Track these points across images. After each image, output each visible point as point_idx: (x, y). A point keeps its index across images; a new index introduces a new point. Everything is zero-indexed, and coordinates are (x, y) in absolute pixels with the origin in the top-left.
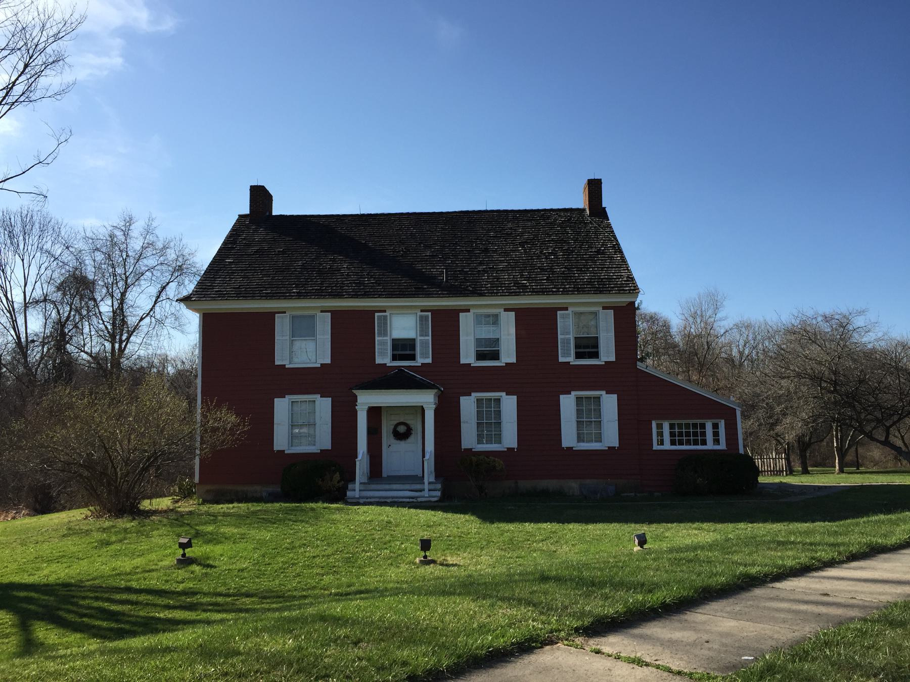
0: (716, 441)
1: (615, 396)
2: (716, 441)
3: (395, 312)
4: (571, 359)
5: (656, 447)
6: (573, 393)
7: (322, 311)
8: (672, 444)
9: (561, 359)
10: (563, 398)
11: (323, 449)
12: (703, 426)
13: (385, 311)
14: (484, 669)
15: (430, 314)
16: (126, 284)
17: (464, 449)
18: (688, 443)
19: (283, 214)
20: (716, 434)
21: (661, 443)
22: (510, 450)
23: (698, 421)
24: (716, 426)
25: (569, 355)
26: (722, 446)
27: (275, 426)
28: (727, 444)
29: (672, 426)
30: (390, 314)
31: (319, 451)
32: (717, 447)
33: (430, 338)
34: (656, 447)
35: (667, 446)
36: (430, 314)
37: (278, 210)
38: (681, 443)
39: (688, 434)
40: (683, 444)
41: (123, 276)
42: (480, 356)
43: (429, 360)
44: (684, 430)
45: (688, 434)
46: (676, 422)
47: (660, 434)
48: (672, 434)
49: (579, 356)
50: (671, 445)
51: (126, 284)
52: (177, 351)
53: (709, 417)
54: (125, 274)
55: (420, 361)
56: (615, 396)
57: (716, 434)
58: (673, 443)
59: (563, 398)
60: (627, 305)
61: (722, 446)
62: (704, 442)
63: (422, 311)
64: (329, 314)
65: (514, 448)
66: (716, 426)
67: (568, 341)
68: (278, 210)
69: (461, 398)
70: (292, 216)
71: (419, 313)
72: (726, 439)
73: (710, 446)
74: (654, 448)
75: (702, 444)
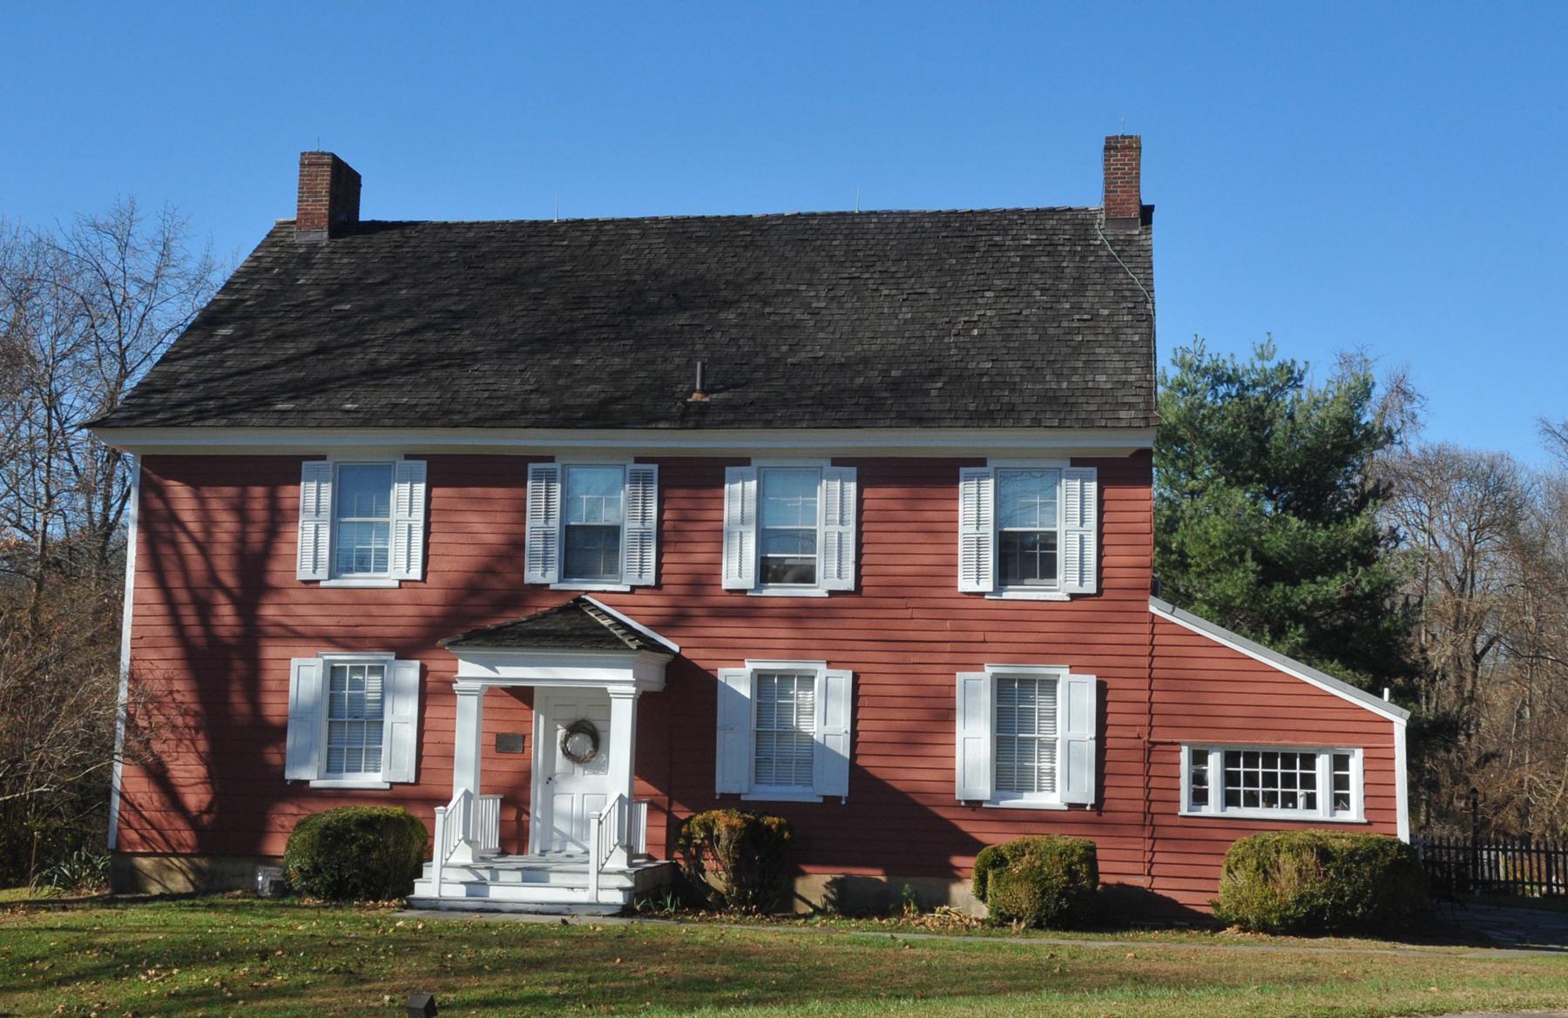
0: (1340, 801)
2: (1340, 801)
3: (574, 462)
7: (408, 457)
11: (726, 792)
13: (551, 459)
15: (655, 468)
16: (123, 365)
17: (722, 795)
19: (377, 219)
20: (1341, 782)
21: (1200, 797)
22: (831, 801)
26: (1355, 812)
27: (719, 734)
30: (563, 466)
31: (821, 800)
32: (1342, 816)
36: (655, 468)
37: (370, 209)
38: (1252, 801)
39: (1270, 780)
41: (115, 348)
45: (1270, 780)
47: (1199, 779)
48: (1230, 779)
51: (123, 365)
54: (120, 343)
57: (1341, 782)
58: (1230, 799)
60: (1131, 456)
61: (1355, 812)
63: (638, 460)
64: (424, 463)
65: (840, 798)
66: (1340, 762)
68: (370, 209)
70: (380, 222)
71: (632, 466)
73: (1322, 812)
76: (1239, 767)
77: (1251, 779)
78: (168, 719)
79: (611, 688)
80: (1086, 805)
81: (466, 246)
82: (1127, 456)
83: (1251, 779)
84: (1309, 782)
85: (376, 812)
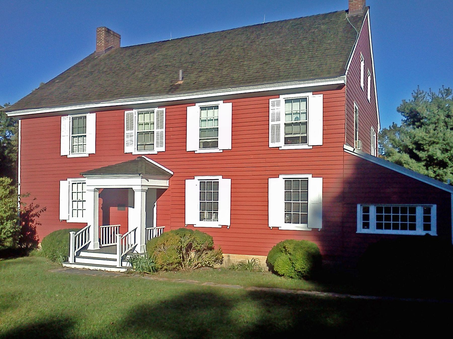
1: (321, 180)
2: (427, 227)
4: (281, 144)
5: (360, 230)
6: (197, 178)
8: (379, 226)
9: (271, 145)
10: (271, 181)
12: (413, 211)
14: (22, 329)
18: (396, 227)
20: (427, 219)
21: (366, 225)
22: (224, 227)
23: (408, 206)
24: (427, 211)
25: (278, 141)
28: (438, 231)
29: (379, 210)
33: (164, 130)
34: (360, 230)
35: (373, 230)
38: (388, 227)
39: (396, 218)
40: (398, 229)
42: (205, 145)
43: (163, 149)
44: (408, 215)
45: (396, 218)
46: (384, 206)
47: (366, 217)
48: (379, 218)
49: (286, 143)
50: (364, 228)
52: (416, 92)
53: (420, 201)
55: (157, 150)
56: (321, 180)
58: (379, 226)
59: (271, 181)
61: (433, 232)
62: (413, 227)
66: (427, 211)
67: (278, 126)
69: (187, 181)
72: (356, 223)
73: (420, 231)
74: (358, 232)
75: (411, 229)
76: (399, 213)
77: (388, 218)
78: (106, 27)
79: (134, 188)
80: (318, 229)
81: (296, 77)
82: (145, 179)
83: (388, 218)
84: (413, 219)
85: (342, 297)
